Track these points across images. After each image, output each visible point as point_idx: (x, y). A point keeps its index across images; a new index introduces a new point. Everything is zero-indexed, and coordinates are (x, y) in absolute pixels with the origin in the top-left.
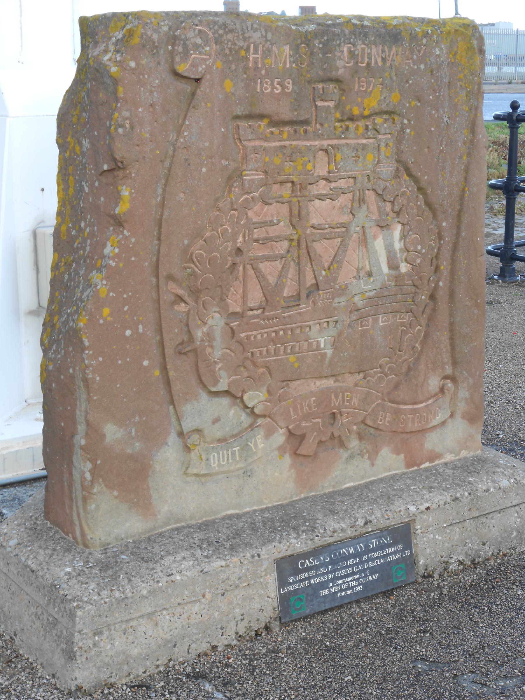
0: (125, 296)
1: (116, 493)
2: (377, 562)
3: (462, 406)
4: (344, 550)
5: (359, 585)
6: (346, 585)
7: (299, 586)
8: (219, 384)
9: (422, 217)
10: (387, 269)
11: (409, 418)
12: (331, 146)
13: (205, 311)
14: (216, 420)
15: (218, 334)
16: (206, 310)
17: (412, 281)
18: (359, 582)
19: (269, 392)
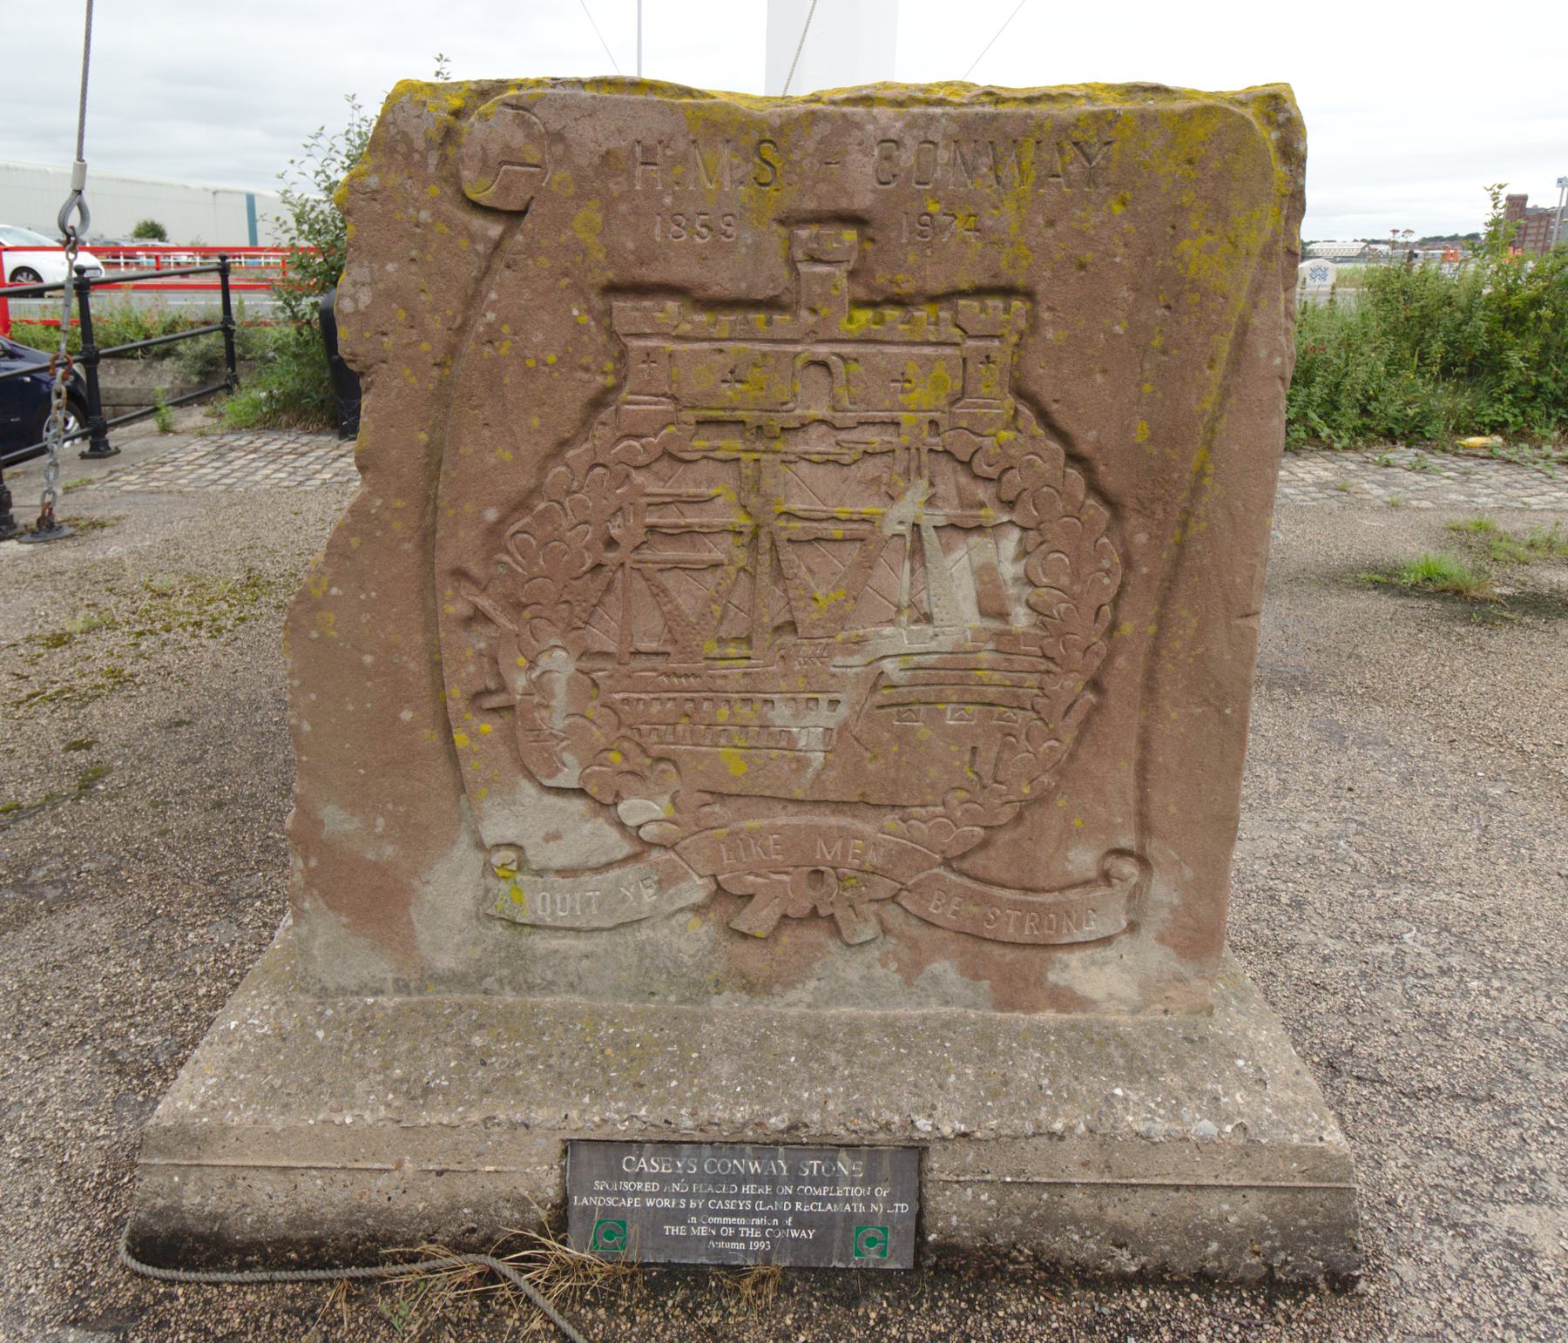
0: (363, 597)
1: (344, 920)
2: (815, 1207)
3: (1158, 918)
4: (735, 1162)
5: (764, 1238)
6: (731, 1231)
7: (615, 1202)
8: (560, 775)
9: (1079, 519)
10: (977, 616)
11: (1009, 916)
12: (839, 356)
13: (534, 642)
14: (554, 836)
15: (560, 688)
16: (537, 641)
17: (1041, 648)
18: (763, 1233)
19: (673, 801)
